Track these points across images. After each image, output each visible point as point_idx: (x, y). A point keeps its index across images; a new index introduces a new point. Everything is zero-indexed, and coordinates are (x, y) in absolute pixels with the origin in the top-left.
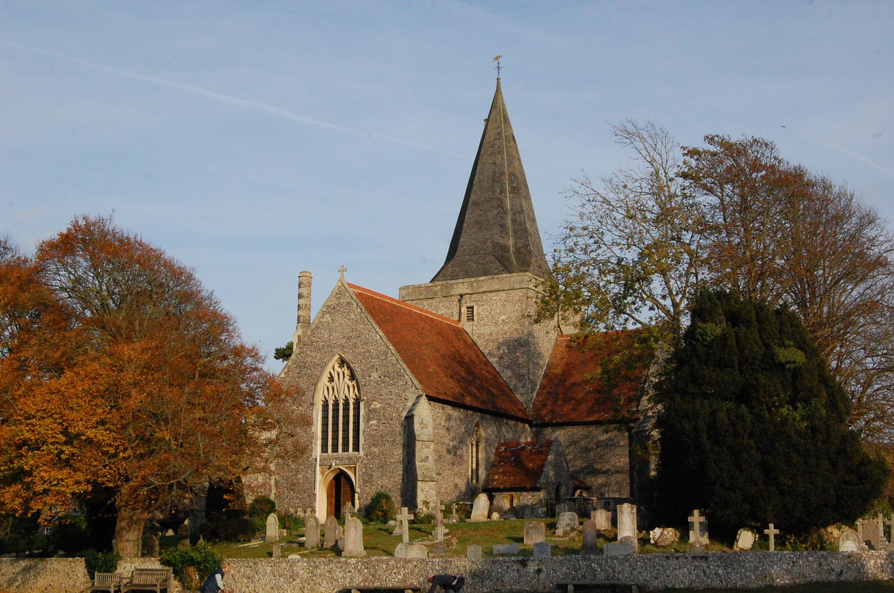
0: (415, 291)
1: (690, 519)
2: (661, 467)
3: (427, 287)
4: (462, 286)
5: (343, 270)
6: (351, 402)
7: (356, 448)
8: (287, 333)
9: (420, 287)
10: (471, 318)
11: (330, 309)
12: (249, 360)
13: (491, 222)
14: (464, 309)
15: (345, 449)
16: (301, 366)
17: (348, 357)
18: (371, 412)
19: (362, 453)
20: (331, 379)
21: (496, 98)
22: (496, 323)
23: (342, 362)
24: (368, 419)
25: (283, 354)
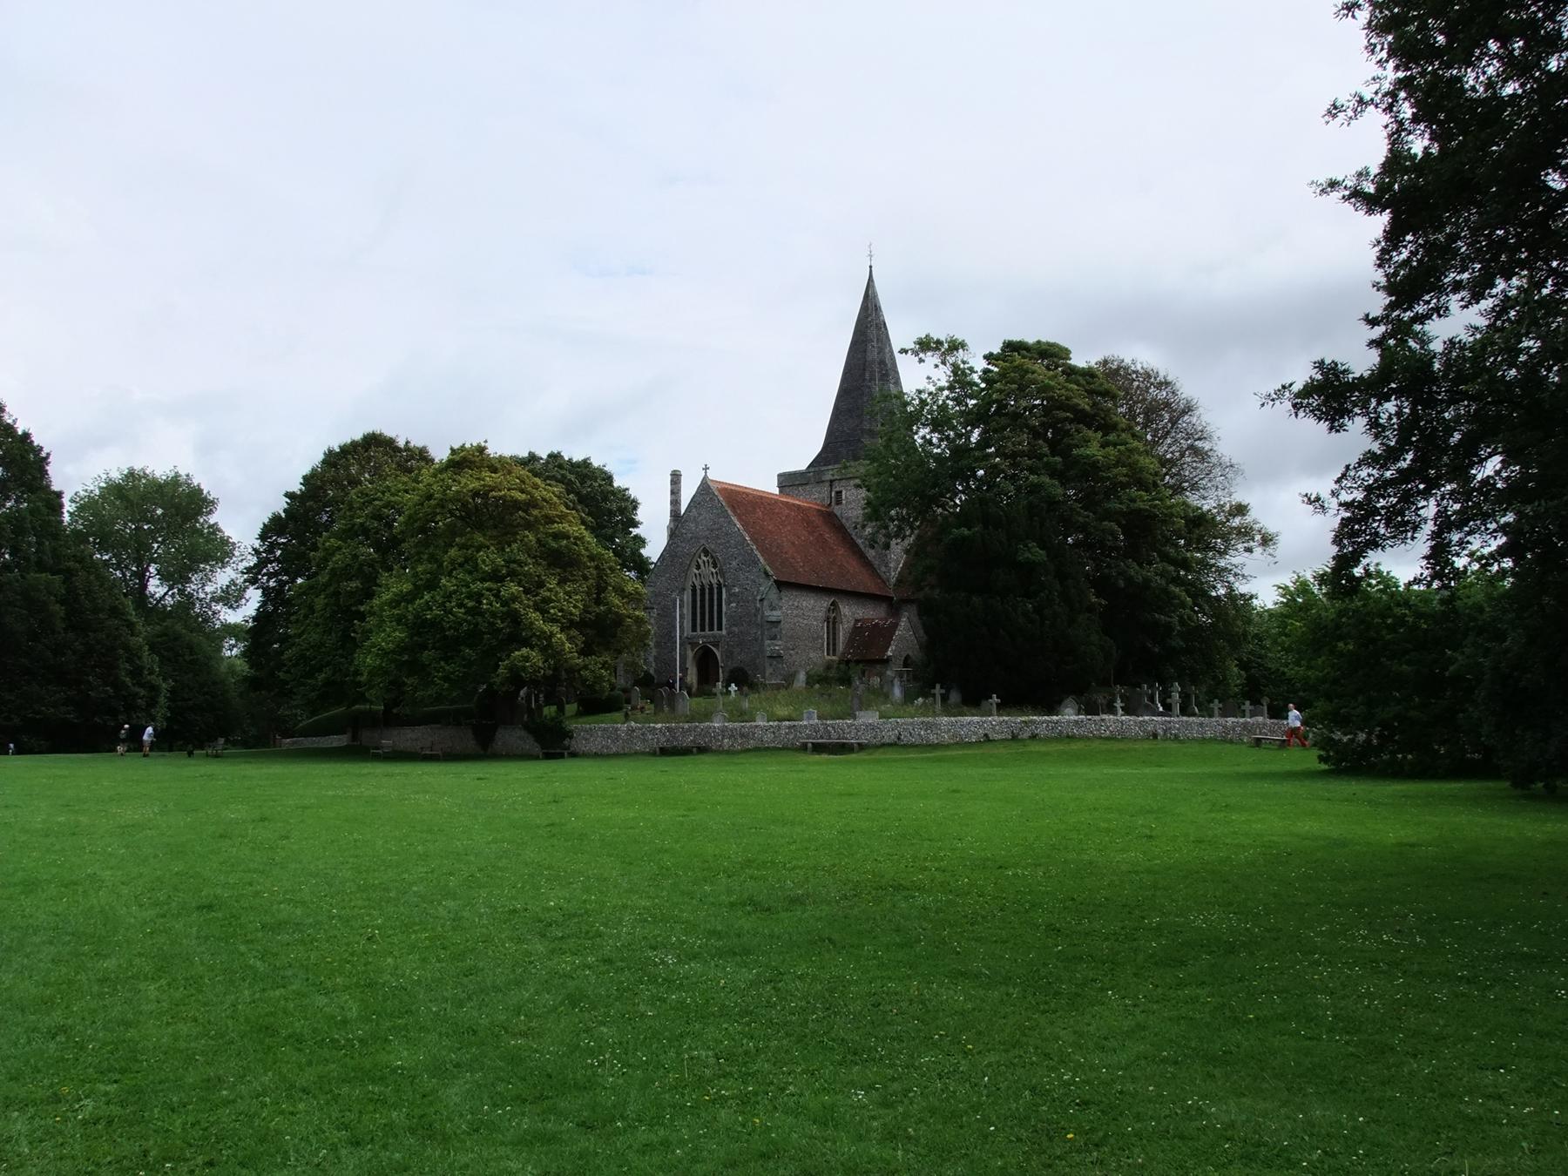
7: (720, 628)
10: (839, 502)
18: (730, 595)
19: (724, 632)
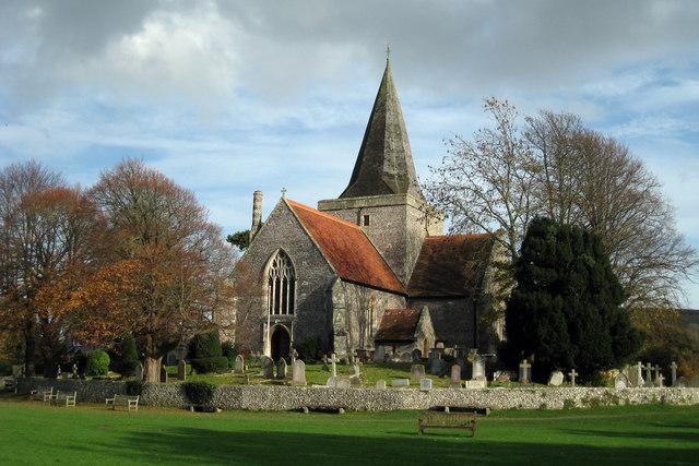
0: (326, 206)
1: (557, 378)
2: (508, 330)
3: (336, 201)
4: (361, 202)
5: (284, 191)
6: (288, 280)
7: (291, 312)
8: (244, 224)
9: (332, 201)
10: (367, 223)
11: (273, 217)
12: (163, 200)
13: (377, 169)
14: (362, 218)
15: (284, 312)
16: (254, 255)
17: (287, 250)
19: (295, 315)
20: (275, 265)
21: (385, 75)
22: (385, 228)
23: (282, 253)
24: (299, 295)
25: (240, 239)
